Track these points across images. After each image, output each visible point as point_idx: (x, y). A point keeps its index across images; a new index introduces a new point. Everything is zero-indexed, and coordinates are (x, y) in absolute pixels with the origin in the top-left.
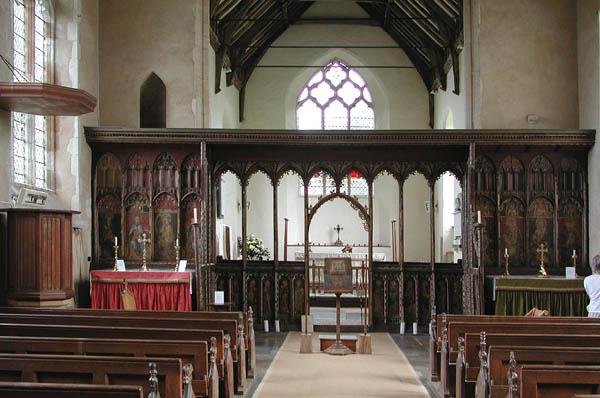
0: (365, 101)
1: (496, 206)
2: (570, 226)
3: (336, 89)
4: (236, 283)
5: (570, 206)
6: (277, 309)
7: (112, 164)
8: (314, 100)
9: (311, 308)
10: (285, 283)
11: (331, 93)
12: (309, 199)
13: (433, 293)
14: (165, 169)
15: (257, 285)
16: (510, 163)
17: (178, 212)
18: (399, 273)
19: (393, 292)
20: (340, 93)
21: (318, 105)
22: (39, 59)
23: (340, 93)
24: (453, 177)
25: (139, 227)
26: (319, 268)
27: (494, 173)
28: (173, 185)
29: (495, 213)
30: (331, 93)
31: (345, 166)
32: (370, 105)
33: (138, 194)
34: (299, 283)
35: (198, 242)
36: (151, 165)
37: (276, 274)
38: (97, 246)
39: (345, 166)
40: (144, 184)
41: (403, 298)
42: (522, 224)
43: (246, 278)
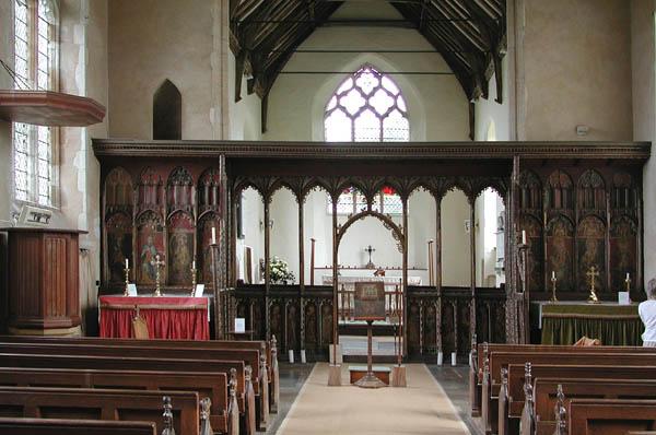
0: (399, 110)
1: (542, 225)
2: (623, 247)
3: (367, 97)
4: (258, 310)
5: (624, 225)
6: (303, 337)
7: (123, 179)
8: (343, 109)
9: (340, 337)
10: (312, 309)
11: (362, 102)
12: (338, 218)
13: (473, 321)
14: (181, 185)
15: (281, 312)
16: (557, 178)
17: (195, 231)
18: (436, 298)
19: (429, 319)
20: (372, 102)
21: (348, 115)
22: (43, 64)
23: (372, 102)
24: (495, 193)
25: (152, 249)
26: (349, 292)
27: (540, 189)
28: (189, 203)
29: (541, 233)
30: (362, 102)
31: (377, 182)
32: (404, 115)
33: (151, 212)
34: (327, 310)
35: (216, 264)
36: (165, 180)
37: (302, 299)
38: (106, 269)
39: (377, 182)
40: (158, 201)
41: (440, 325)
42: (571, 245)
43: (269, 304)
